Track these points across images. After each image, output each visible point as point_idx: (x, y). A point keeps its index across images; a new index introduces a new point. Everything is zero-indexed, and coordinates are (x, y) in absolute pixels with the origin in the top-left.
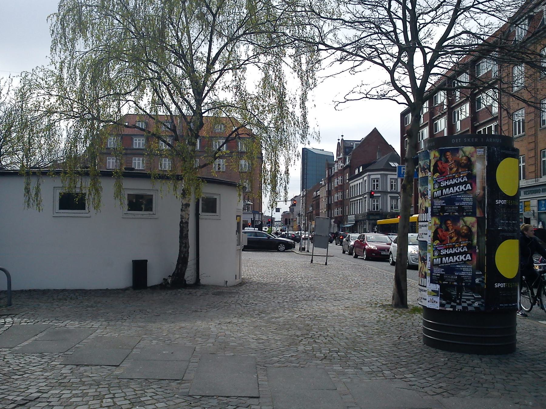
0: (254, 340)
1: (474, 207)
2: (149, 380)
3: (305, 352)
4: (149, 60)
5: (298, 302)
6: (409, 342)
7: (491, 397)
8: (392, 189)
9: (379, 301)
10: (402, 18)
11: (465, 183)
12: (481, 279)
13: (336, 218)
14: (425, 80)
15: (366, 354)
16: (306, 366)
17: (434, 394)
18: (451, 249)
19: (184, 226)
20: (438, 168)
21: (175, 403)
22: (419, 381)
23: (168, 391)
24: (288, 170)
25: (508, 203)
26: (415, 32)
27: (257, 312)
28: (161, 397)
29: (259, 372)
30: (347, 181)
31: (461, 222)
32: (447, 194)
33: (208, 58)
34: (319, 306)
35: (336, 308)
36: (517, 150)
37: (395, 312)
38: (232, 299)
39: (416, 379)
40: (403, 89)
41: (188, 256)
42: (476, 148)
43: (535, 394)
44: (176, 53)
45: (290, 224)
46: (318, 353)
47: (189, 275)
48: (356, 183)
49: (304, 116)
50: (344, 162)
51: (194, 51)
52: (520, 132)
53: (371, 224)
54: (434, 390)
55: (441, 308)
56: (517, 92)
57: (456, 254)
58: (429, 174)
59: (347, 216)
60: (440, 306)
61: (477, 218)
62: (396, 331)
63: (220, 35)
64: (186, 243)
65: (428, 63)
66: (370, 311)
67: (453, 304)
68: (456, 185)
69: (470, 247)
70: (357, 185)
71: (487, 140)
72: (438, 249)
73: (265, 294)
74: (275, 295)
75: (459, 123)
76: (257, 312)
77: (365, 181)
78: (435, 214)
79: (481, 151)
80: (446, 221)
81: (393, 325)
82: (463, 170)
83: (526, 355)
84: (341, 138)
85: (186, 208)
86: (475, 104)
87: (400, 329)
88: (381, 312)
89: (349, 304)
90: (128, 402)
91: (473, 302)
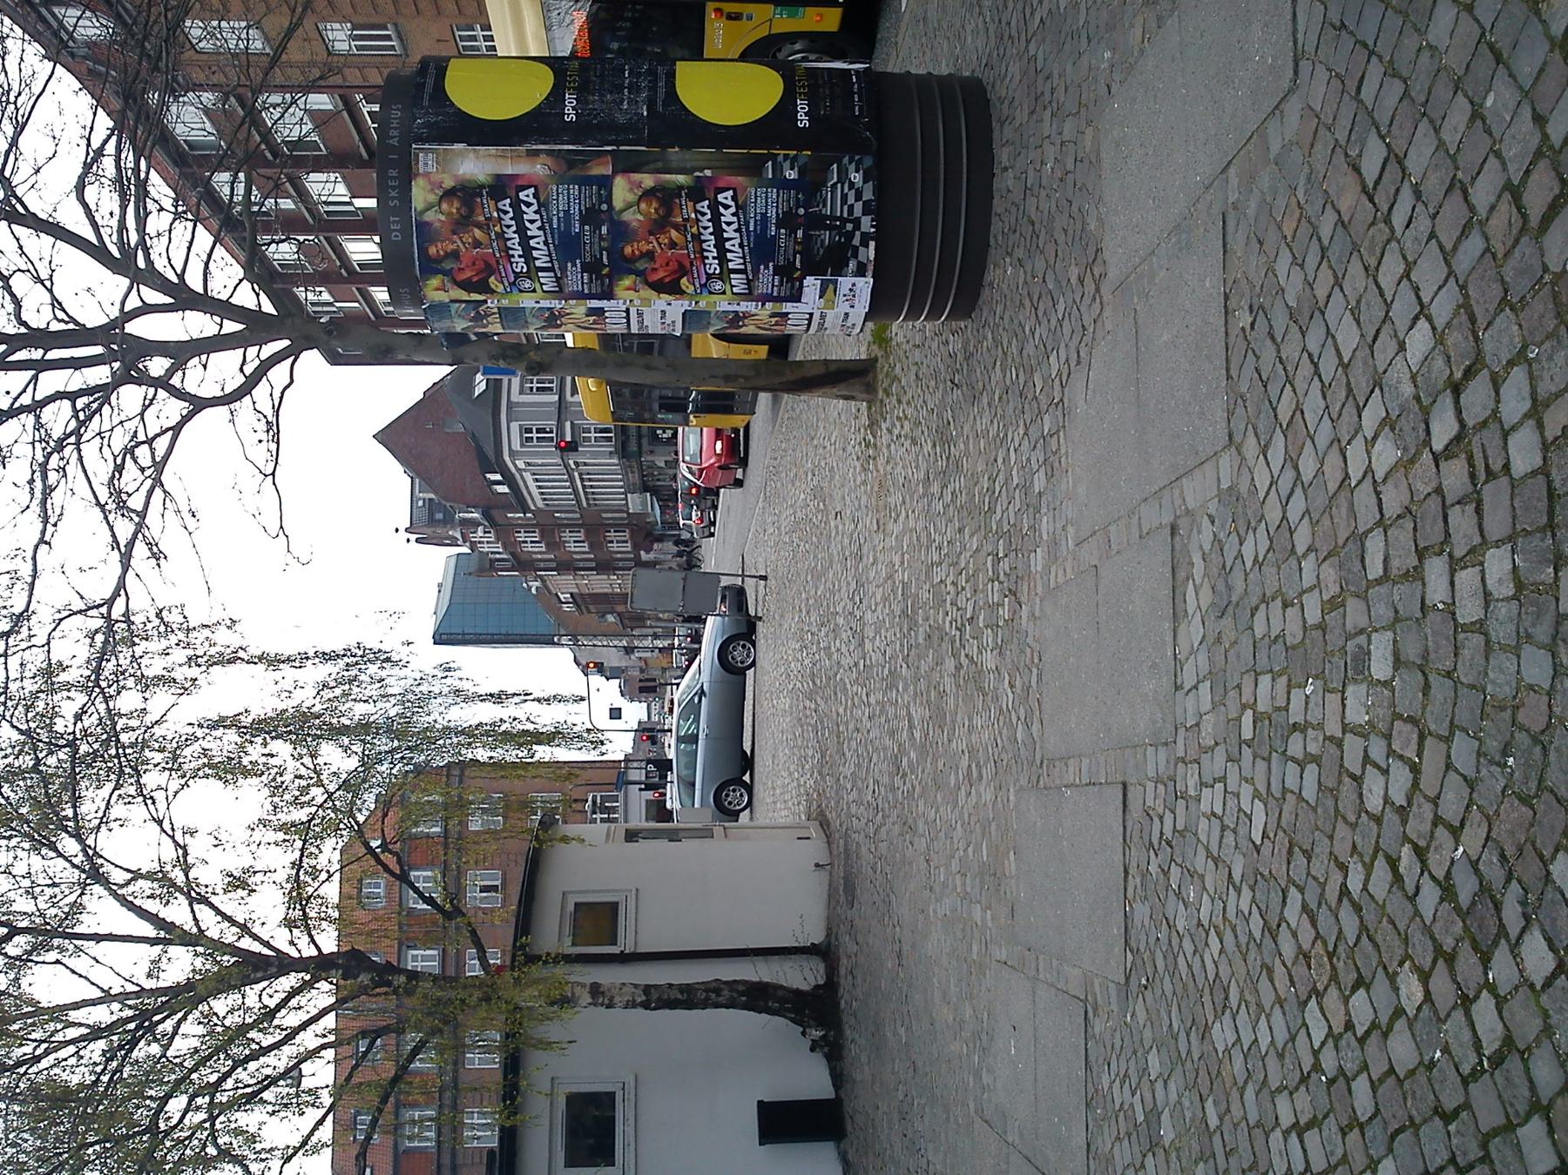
0: (973, 791)
1: (585, 181)
2: (1090, 1096)
3: (1000, 650)
4: (153, 1128)
5: (868, 662)
6: (967, 359)
7: (1098, 154)
8: (550, 389)
9: (860, 437)
10: (33, 372)
11: (517, 204)
12: (787, 164)
13: (637, 547)
14: (224, 309)
15: (1001, 477)
16: (1036, 646)
17: (1098, 300)
18: (705, 246)
19: (656, 999)
20: (475, 279)
21: (1149, 1023)
22: (1067, 338)
23: (1118, 1043)
24: (491, 695)
25: (574, 88)
26: (81, 335)
27: (898, 781)
28: (1132, 1062)
29: (1058, 782)
30: (529, 515)
31: (628, 216)
32: (550, 255)
33: (153, 942)
34: (876, 604)
35: (880, 557)
36: (425, 63)
37: (887, 393)
38: (864, 850)
39: (1063, 345)
40: (248, 369)
41: (746, 982)
42: (418, 175)
43: (1084, 40)
44: (134, 1043)
45: (654, 680)
46: (1001, 613)
47: (800, 976)
48: (535, 492)
49: (327, 657)
50: (474, 524)
51: (131, 988)
52: (388, 38)
53: (651, 448)
54: (1087, 300)
55: (870, 273)
56: (267, 39)
57: (718, 232)
58: (492, 304)
59: (629, 514)
60: (864, 276)
61: (615, 173)
62: (939, 395)
63: (77, 908)
64: (707, 991)
65: (172, 301)
66: (888, 462)
67: (856, 241)
68: (522, 231)
69: (697, 192)
70: (540, 487)
71: (394, 142)
72: (703, 281)
73: (848, 755)
74: (851, 727)
75: (360, 203)
76: (898, 781)
77: (529, 464)
78: (605, 288)
79: (426, 161)
81: (921, 400)
82: (479, 210)
83: (988, 51)
84: (403, 535)
85: (603, 993)
86: (300, 159)
87: (933, 383)
88: (890, 431)
89: (869, 522)
90: (1149, 1160)
91: (852, 185)
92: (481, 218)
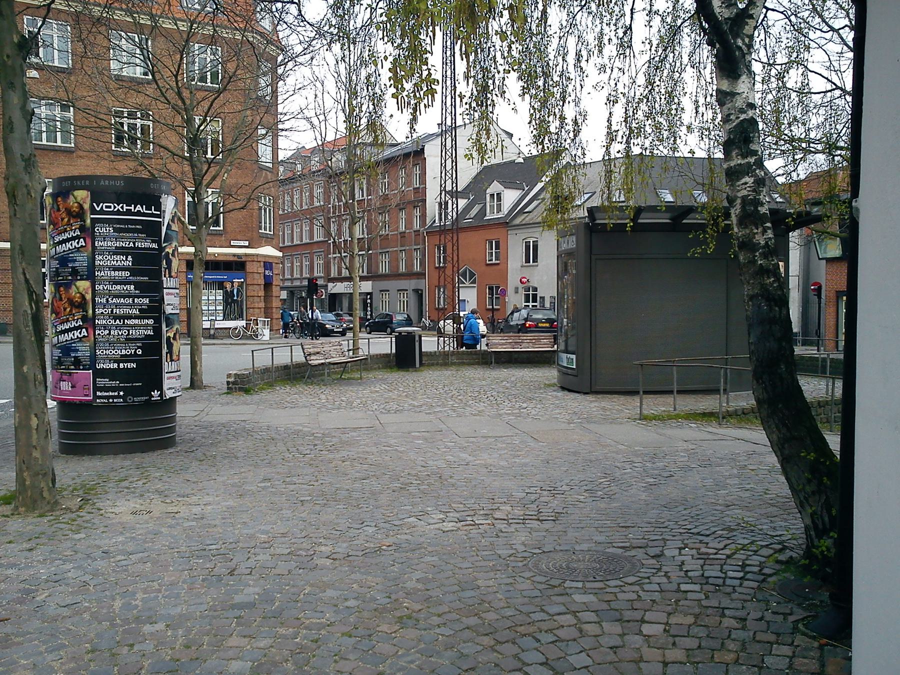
71: (102, 183)
80: (59, 287)
92: (74, 312)
